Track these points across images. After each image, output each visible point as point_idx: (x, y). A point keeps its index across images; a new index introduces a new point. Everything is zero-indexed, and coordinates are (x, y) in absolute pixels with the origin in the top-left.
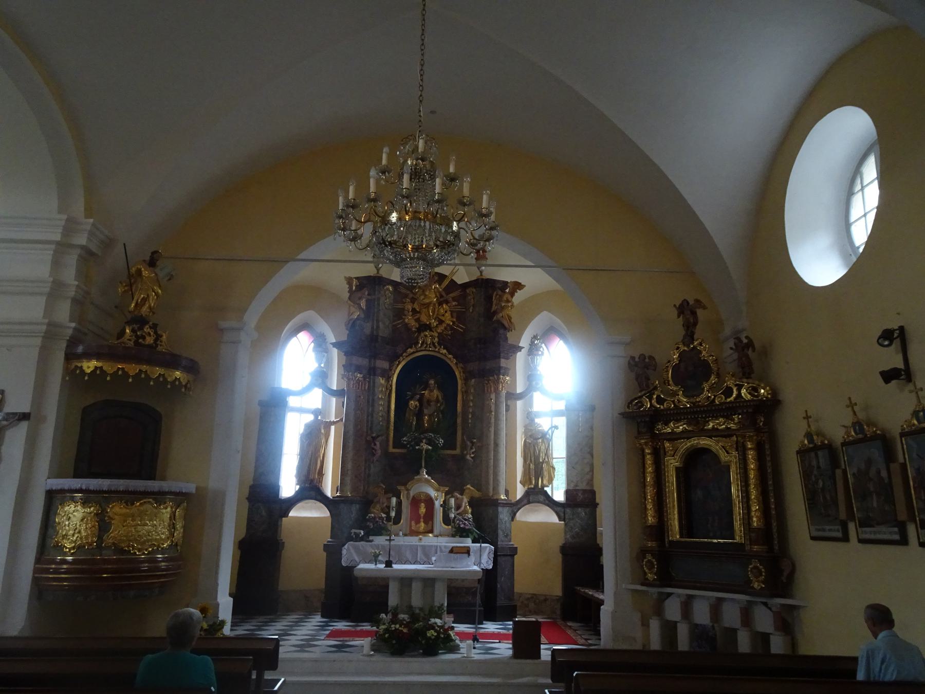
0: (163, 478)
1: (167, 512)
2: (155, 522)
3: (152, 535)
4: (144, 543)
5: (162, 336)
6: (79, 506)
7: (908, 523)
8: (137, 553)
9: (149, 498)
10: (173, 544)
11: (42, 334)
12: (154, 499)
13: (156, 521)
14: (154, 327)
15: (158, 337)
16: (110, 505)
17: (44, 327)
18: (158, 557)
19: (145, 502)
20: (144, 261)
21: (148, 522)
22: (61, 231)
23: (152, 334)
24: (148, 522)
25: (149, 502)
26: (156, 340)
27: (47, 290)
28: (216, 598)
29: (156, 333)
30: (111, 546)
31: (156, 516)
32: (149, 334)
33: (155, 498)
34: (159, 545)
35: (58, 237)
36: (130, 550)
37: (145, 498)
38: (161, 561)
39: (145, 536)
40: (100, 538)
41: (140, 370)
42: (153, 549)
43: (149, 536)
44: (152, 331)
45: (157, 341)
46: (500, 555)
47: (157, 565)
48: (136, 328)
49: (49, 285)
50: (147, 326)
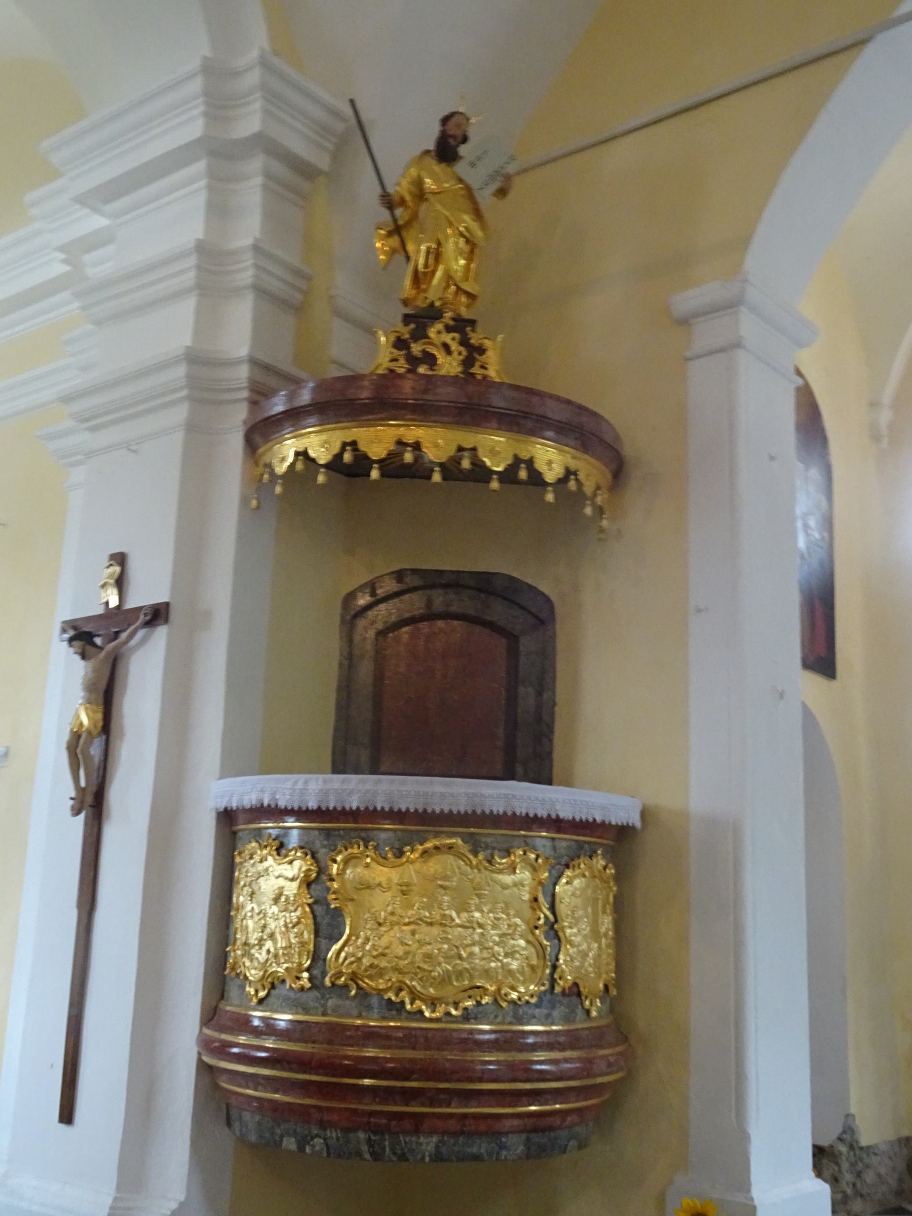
0: (568, 782)
1: (518, 884)
2: (477, 915)
3: (471, 954)
4: (445, 979)
5: (481, 350)
6: (270, 858)
7: (260, 991)
8: (427, 1014)
9: (452, 835)
10: (558, 989)
11: (185, 393)
12: (469, 839)
13: (482, 911)
14: (461, 326)
15: (474, 352)
16: (337, 854)
17: (180, 371)
18: (524, 1032)
19: (436, 848)
20: (427, 152)
21: (454, 914)
22: (202, 108)
23: (454, 346)
24: (454, 914)
25: (450, 847)
26: (468, 363)
27: (190, 278)
28: (745, 1185)
29: (465, 342)
30: (346, 987)
31: (479, 896)
32: (446, 348)
33: (472, 834)
34: (499, 990)
35: (195, 129)
36: (402, 1003)
37: (437, 835)
38: (534, 1047)
39: (448, 958)
40: (318, 957)
41: (400, 443)
42: (479, 1003)
43: (460, 957)
44: (453, 339)
45: (473, 366)
46: (181, 388)
47: (469, 1057)
48: (407, 336)
49: (192, 261)
50: (439, 326)
